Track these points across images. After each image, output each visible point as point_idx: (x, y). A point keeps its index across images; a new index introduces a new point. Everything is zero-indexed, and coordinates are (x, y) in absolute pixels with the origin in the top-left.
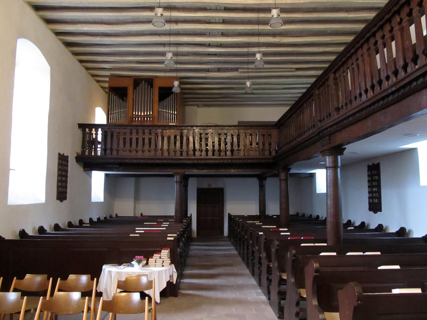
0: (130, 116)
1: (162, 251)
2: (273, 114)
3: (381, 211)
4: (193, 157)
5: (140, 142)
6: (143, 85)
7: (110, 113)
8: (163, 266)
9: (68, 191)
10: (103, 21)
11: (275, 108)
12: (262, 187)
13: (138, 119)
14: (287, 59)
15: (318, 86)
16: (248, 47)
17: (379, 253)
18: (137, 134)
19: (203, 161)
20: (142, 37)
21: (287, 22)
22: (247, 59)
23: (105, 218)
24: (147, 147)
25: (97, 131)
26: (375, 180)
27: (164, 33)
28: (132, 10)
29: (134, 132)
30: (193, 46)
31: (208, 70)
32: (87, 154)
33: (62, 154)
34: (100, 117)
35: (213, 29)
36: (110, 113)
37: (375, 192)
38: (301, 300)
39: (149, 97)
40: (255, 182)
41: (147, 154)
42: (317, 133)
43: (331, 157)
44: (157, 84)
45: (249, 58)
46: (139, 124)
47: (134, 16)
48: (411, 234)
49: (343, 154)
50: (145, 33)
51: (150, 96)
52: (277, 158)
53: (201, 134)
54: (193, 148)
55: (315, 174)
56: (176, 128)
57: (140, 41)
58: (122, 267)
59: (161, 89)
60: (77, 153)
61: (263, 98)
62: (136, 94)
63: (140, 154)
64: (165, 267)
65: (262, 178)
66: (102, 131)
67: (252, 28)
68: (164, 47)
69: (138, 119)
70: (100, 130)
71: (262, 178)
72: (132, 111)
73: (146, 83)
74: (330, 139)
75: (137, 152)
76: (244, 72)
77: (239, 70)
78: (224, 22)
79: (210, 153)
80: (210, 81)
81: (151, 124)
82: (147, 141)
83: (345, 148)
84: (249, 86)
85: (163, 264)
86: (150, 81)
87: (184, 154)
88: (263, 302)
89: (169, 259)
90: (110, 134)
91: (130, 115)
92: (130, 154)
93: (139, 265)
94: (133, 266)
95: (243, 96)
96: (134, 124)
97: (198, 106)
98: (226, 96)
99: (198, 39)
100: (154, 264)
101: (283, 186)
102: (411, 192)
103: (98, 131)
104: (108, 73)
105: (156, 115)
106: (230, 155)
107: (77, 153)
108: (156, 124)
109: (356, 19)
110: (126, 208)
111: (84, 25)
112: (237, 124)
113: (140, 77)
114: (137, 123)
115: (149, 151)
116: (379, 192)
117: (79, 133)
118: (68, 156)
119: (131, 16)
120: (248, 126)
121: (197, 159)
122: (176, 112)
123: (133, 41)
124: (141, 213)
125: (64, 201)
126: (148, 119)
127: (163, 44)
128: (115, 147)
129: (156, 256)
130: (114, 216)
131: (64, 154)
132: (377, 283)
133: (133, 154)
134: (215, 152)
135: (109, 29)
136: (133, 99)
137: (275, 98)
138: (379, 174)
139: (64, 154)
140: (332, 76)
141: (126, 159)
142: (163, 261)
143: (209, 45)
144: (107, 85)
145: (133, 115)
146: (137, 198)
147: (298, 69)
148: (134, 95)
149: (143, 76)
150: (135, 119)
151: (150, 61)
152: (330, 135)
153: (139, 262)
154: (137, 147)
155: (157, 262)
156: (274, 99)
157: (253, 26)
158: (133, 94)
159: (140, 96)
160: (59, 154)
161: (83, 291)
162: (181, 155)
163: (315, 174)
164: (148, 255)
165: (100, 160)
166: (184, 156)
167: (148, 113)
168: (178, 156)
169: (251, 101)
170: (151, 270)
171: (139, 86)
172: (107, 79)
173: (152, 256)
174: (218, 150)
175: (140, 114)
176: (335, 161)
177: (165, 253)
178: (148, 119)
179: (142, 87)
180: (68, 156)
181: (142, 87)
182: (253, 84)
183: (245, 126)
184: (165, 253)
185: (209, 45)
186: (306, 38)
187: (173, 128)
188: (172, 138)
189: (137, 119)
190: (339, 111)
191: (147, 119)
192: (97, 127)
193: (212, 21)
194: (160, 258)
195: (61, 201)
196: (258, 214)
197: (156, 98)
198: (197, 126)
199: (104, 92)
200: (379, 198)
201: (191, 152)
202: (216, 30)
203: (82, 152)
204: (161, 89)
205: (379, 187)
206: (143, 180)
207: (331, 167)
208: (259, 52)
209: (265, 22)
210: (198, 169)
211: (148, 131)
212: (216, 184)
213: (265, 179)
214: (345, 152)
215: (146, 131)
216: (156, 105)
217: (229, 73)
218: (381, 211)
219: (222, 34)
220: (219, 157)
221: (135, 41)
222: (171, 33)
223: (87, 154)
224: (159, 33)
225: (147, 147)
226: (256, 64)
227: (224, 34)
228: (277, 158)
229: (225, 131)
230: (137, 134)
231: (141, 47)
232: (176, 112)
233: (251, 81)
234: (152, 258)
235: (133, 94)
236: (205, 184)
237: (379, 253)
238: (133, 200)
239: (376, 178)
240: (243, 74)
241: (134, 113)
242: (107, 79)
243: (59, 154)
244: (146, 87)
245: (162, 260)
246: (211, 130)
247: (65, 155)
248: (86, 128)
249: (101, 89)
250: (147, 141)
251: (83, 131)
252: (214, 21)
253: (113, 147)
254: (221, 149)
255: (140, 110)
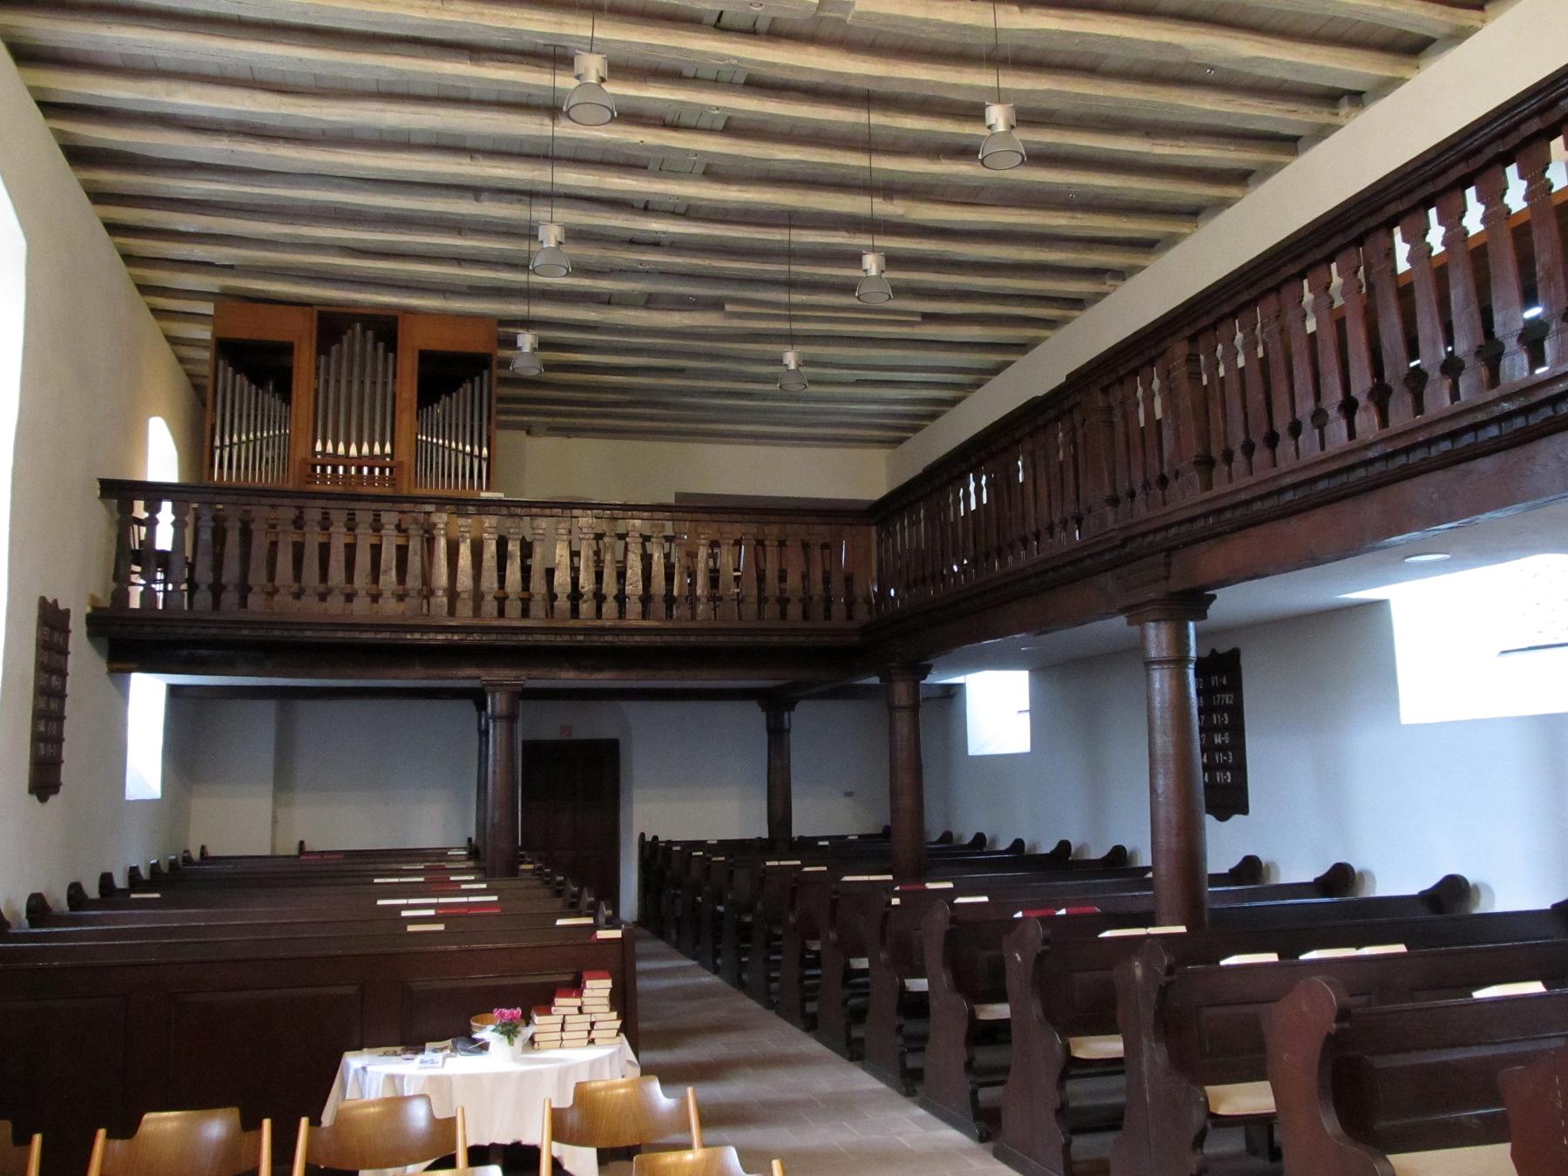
0: (304, 460)
1: (589, 983)
2: (863, 476)
3: (1244, 810)
4: (572, 623)
5: (363, 559)
6: (356, 339)
7: (217, 443)
8: (592, 1042)
9: (67, 751)
10: (258, 76)
11: (848, 451)
12: (777, 735)
13: (335, 470)
14: (907, 281)
15: (1106, 381)
16: (791, 227)
17: (1401, 948)
18: (351, 529)
19: (608, 638)
20: (404, 156)
21: (1037, 158)
22: (785, 268)
23: (154, 868)
24: (389, 578)
25: (153, 508)
26: (1222, 709)
27: (490, 146)
28: (396, 47)
29: (339, 518)
30: (586, 205)
31: (607, 300)
32: (135, 603)
33: (50, 600)
34: (161, 458)
35: (686, 151)
36: (217, 443)
37: (1222, 748)
38: (1215, 1125)
39: (356, 387)
40: (752, 717)
41: (390, 608)
42: (1118, 543)
43: (1163, 625)
44: (414, 340)
45: (794, 268)
46: (339, 489)
47: (402, 73)
48: (1368, 883)
49: (1204, 617)
50: (414, 139)
51: (385, 384)
52: (847, 627)
53: (599, 537)
54: (663, 592)
55: (961, 686)
56: (504, 511)
57: (390, 170)
58: (428, 1055)
59: (426, 358)
60: (93, 599)
61: (783, 411)
62: (327, 373)
63: (310, 607)
64: (602, 1046)
65: (776, 704)
66: (175, 511)
67: (827, 160)
68: (477, 200)
69: (335, 470)
70: (167, 506)
71: (776, 704)
72: (310, 438)
73: (370, 334)
74: (1168, 565)
75: (349, 598)
76: (739, 316)
77: (728, 308)
78: (733, 128)
79: (634, 607)
80: (708, 344)
81: (387, 490)
82: (389, 555)
83: (1214, 597)
84: (792, 366)
85: (594, 1034)
86: (385, 328)
87: (538, 608)
88: (966, 1152)
89: (614, 1015)
90: (238, 525)
91: (301, 452)
92: (298, 604)
93: (511, 1042)
94: (484, 1047)
95: (687, 400)
96: (317, 486)
97: (529, 432)
98: (649, 399)
99: (617, 180)
100: (557, 1036)
101: (903, 728)
102: (1364, 747)
103: (158, 509)
104: (212, 283)
105: (405, 455)
106: (616, 615)
107: (93, 599)
108: (405, 493)
109: (1177, 162)
110: (241, 824)
111: (176, 86)
112: (671, 500)
113: (348, 306)
114: (329, 487)
115: (401, 598)
116: (1238, 747)
117: (100, 516)
118: (67, 612)
119: (392, 71)
120: (706, 510)
121: (587, 631)
122: (485, 451)
123: (365, 168)
124: (302, 843)
125: (52, 799)
126: (377, 471)
127: (530, 195)
128: (258, 577)
129: (564, 1005)
130: (196, 855)
131: (55, 601)
132: (1463, 1045)
133: (335, 605)
134: (652, 606)
135: (284, 111)
136: (317, 391)
137: (811, 413)
138: (1236, 687)
139: (55, 601)
140: (1180, 349)
141: (302, 626)
142: (592, 1024)
143: (647, 208)
144: (204, 333)
145: (315, 454)
146: (283, 781)
147: (929, 318)
148: (317, 377)
149: (356, 304)
150: (324, 470)
151: (403, 248)
152: (1169, 551)
153: (509, 1031)
154: (350, 578)
155: (568, 1027)
156: (812, 419)
157: (827, 152)
158: (317, 374)
159: (332, 382)
160: (43, 600)
161: (603, 1146)
162: (525, 613)
163: (961, 686)
164: (537, 1000)
165: (194, 631)
166: (538, 618)
167: (377, 450)
168: (513, 618)
169: (725, 422)
170: (561, 1060)
171: (340, 342)
172: (207, 308)
173: (546, 1006)
174: (616, 597)
175: (341, 449)
176: (1180, 640)
177: (598, 989)
178: (377, 471)
179: (352, 346)
180: (67, 612)
181: (352, 346)
182: (805, 362)
183: (706, 510)
184: (598, 989)
185: (647, 208)
186: (992, 210)
187: (492, 509)
188: (491, 549)
189: (329, 469)
190: (1210, 471)
191: (371, 471)
192: (155, 493)
193: (685, 120)
194: (580, 1010)
195: (43, 799)
196: (765, 835)
197: (408, 391)
198: (586, 506)
199: (173, 357)
200: (1240, 769)
201: (563, 603)
202: (696, 153)
203: (114, 598)
204: (426, 358)
205: (1237, 730)
206: (304, 707)
207: (1168, 662)
208: (873, 249)
209: (965, 151)
210: (578, 667)
211: (369, 517)
212: (592, 724)
213: (791, 706)
214: (1214, 610)
215: (359, 516)
216: (406, 419)
217: (686, 314)
218: (1244, 810)
219: (705, 173)
220: (669, 625)
221: (373, 169)
222: (557, 153)
223: (135, 603)
224: (469, 143)
225: (389, 578)
226: (862, 290)
227: (713, 172)
228: (847, 627)
229: (621, 527)
230: (351, 529)
231: (383, 193)
232: (485, 451)
233: (800, 348)
234: (550, 1013)
235: (317, 374)
236: (548, 724)
237: (1401, 948)
238: (269, 788)
239: (1228, 699)
240: (736, 323)
241: (319, 447)
242: (207, 308)
243: (43, 600)
244: (369, 347)
245: (587, 1018)
246: (638, 522)
247: (62, 606)
248: (122, 493)
249: (167, 346)
250: (389, 555)
251: (120, 509)
252: (693, 122)
253: (251, 581)
254: (675, 593)
255: (377, 436)
